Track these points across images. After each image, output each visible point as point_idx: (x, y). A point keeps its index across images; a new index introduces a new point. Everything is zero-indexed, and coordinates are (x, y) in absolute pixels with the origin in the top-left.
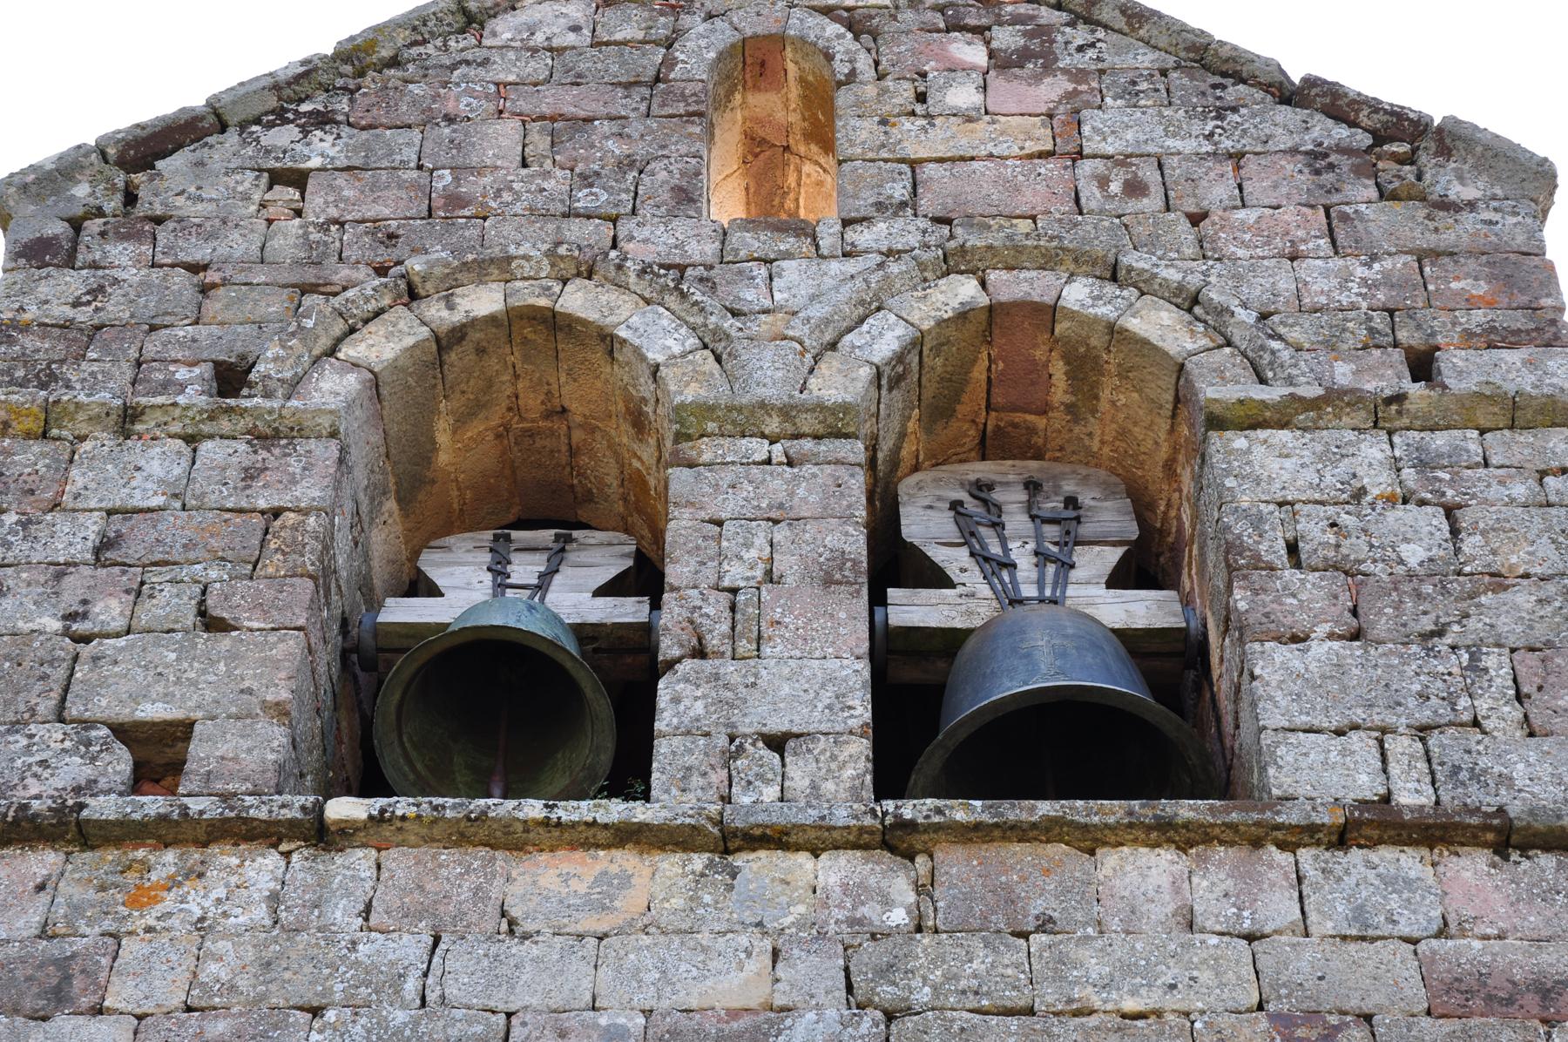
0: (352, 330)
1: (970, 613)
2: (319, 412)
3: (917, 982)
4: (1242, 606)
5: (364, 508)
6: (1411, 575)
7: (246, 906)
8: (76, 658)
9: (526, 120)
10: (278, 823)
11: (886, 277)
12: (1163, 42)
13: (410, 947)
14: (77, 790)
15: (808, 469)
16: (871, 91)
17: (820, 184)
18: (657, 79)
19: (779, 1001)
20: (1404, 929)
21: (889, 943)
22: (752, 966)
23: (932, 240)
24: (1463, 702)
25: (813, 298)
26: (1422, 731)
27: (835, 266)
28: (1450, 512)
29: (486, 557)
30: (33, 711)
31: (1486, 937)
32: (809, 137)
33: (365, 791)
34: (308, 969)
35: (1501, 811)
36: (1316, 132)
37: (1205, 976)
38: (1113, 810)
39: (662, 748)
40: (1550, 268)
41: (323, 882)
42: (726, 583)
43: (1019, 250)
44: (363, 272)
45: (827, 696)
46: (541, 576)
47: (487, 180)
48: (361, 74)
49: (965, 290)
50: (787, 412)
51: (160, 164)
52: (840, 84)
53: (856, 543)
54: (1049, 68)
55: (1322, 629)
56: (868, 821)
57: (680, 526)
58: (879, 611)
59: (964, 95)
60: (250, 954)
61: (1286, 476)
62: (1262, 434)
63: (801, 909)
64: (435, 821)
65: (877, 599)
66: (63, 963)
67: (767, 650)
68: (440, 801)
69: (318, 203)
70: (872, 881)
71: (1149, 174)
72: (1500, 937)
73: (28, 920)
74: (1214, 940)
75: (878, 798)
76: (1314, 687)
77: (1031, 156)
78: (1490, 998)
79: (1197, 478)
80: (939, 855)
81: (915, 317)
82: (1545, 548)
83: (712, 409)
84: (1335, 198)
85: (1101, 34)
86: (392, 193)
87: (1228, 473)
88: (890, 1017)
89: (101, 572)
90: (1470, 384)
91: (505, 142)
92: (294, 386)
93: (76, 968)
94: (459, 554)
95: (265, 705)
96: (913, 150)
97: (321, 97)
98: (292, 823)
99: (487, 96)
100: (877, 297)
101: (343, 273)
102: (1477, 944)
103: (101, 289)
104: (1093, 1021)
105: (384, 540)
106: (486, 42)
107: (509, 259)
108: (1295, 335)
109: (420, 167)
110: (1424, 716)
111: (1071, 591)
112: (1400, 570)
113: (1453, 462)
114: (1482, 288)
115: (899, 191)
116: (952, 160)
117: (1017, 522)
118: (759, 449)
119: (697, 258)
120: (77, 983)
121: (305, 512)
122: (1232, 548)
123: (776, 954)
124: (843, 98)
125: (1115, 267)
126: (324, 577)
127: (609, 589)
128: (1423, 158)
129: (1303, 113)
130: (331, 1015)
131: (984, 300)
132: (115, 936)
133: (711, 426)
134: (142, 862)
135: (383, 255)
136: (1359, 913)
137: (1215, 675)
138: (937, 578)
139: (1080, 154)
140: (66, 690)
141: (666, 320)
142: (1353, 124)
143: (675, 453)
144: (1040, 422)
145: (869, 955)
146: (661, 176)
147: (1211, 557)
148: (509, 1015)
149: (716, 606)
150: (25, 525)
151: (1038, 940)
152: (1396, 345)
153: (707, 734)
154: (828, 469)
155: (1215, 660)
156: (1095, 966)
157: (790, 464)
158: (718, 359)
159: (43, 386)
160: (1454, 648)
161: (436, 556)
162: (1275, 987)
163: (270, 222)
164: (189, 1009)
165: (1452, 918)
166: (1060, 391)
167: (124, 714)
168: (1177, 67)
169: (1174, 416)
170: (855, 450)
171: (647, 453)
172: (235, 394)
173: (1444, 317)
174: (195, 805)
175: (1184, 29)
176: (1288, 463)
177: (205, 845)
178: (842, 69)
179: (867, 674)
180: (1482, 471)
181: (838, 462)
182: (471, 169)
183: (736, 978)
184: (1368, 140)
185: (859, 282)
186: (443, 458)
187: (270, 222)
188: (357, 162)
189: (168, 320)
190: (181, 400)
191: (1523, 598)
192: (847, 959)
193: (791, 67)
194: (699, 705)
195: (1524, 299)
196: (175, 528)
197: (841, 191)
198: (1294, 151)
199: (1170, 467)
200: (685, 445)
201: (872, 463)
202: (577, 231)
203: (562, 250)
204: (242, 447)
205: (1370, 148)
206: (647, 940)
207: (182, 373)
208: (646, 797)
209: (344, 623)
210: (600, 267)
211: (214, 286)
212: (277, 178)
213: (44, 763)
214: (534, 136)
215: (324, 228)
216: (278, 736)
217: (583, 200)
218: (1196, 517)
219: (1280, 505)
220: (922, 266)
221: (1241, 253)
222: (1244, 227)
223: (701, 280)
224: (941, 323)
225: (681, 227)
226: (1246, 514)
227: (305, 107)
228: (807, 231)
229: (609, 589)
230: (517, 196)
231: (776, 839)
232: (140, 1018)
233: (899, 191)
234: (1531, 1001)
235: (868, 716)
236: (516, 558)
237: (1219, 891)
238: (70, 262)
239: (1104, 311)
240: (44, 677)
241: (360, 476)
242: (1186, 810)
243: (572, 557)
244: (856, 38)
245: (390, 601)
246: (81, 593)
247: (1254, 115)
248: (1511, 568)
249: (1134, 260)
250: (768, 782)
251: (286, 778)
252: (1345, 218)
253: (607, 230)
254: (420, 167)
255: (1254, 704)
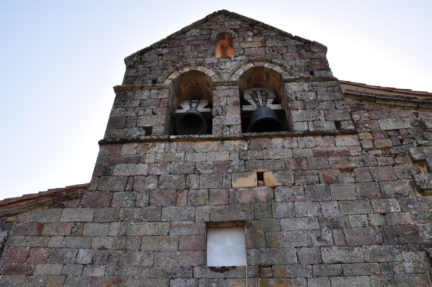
0: (170, 74)
1: (254, 108)
2: (166, 85)
3: (248, 157)
4: (290, 106)
5: (173, 98)
6: (311, 101)
7: (161, 150)
8: (137, 119)
9: (191, 45)
10: (164, 139)
11: (241, 64)
12: (276, 31)
13: (182, 154)
14: (139, 136)
15: (231, 90)
16: (237, 39)
17: (231, 52)
18: (209, 39)
19: (230, 160)
20: (311, 146)
21: (245, 152)
22: (227, 155)
23: (247, 59)
24: (318, 117)
25: (231, 67)
26: (313, 121)
27: (234, 63)
28: (316, 92)
29: (189, 104)
30: (133, 126)
31: (321, 147)
32: (229, 46)
33: (175, 135)
34: (169, 157)
35: (323, 131)
36: (297, 43)
37: (286, 154)
38: (273, 133)
39: (214, 128)
40: (327, 60)
41: (170, 146)
42: (221, 105)
43: (258, 59)
44: (171, 67)
45: (235, 120)
46: (196, 106)
47: (187, 53)
48: (170, 41)
49: (252, 65)
50: (228, 82)
51: (144, 54)
52: (233, 38)
53: (238, 99)
54: (261, 35)
55: (300, 108)
56: (241, 136)
57: (215, 98)
58: (241, 109)
59: (250, 39)
60: (162, 156)
61: (295, 88)
62: (291, 83)
63: (233, 148)
64: (184, 138)
65: (241, 107)
66: (139, 157)
67: (227, 114)
68: (184, 136)
69: (165, 58)
70: (242, 144)
71: (275, 49)
72: (323, 147)
73: (135, 152)
74: (287, 149)
75: (242, 133)
76: (299, 116)
77: (259, 47)
78: (321, 154)
79: (283, 89)
80: (251, 140)
81: (245, 69)
82: (328, 97)
83: (219, 82)
84: (300, 52)
85: (268, 31)
86: (174, 56)
87: (287, 88)
88: (245, 161)
89: (140, 108)
90: (318, 76)
91: (189, 48)
92: (163, 82)
93: (141, 158)
94: (185, 104)
95: (161, 124)
96: (244, 47)
97: (165, 44)
98: (166, 139)
99: (186, 43)
100: (239, 66)
101: (168, 67)
102: (320, 148)
103: (138, 71)
104: (271, 160)
105: (175, 102)
106: (186, 35)
107: (190, 64)
108: (295, 70)
109: (178, 52)
110: (313, 119)
111: (267, 105)
112: (310, 100)
113: (316, 86)
114: (319, 63)
115: (242, 52)
116: (249, 48)
117: (259, 96)
118: (224, 87)
119: (215, 62)
120: (141, 159)
121: (165, 99)
122: (288, 98)
123: (230, 154)
124: (234, 40)
125: (271, 61)
126: (168, 107)
127: (205, 107)
128: (311, 46)
129: (295, 41)
130: (173, 163)
131: (254, 66)
132: (145, 154)
133: (218, 85)
134: (148, 144)
135: (173, 64)
136: (305, 145)
137: (286, 115)
138: (249, 104)
139: (266, 47)
140: (137, 123)
141: (211, 71)
142: (301, 42)
143: (213, 89)
144: (262, 82)
145: (242, 153)
146: (210, 52)
147: (285, 100)
148: (195, 163)
149: (220, 109)
150: (130, 102)
151: (264, 150)
152: (308, 71)
153: (219, 126)
154: (234, 90)
155: (286, 113)
156: (272, 154)
157: (229, 89)
158: (219, 76)
159: (131, 84)
160: (317, 110)
161: (182, 104)
162: (295, 155)
163: (159, 61)
164: (155, 163)
165: (317, 145)
166: (265, 78)
167: (144, 126)
168: (278, 35)
169: (280, 81)
170: (237, 87)
171: (210, 89)
172: (155, 84)
173: (314, 67)
174: (154, 137)
175: (279, 30)
176: (295, 87)
177: (155, 142)
178: (233, 36)
179: (240, 117)
180: (320, 87)
181: (235, 89)
182: (184, 52)
183: (225, 157)
184: (303, 44)
185: (237, 65)
186: (182, 91)
187: (159, 61)
188: (170, 52)
189: (146, 74)
190: (148, 85)
191: (325, 103)
192: (239, 154)
193: (227, 36)
194: (218, 122)
195: (324, 64)
196: (149, 102)
197: (234, 53)
198: (294, 45)
199: (279, 88)
200: (215, 87)
201: (240, 89)
202: (199, 60)
203: (197, 62)
204: (156, 90)
205: (304, 45)
206: (213, 153)
207: (148, 81)
208: (212, 134)
209: (171, 113)
210: (202, 64)
211: (152, 70)
212: (160, 55)
213: (135, 132)
214: (193, 47)
215: (166, 61)
216: (163, 128)
217: (199, 55)
218: (283, 94)
219: (294, 92)
220: (245, 62)
221: (288, 59)
222: (288, 56)
223: (216, 65)
224: (248, 70)
225: (213, 58)
226: (290, 94)
227: (163, 46)
228: (230, 58)
229: (205, 107)
230: (191, 55)
231: (229, 139)
232: (149, 164)
233: (242, 52)
234: (326, 154)
235: (241, 122)
236: (193, 104)
237: (287, 143)
238: (134, 68)
239: (270, 67)
240: (134, 121)
241: (172, 93)
242: (283, 133)
243: (200, 103)
244: (235, 32)
245: (177, 110)
246: (138, 110)
247: (288, 41)
248: (324, 99)
249: (274, 60)
250: (228, 131)
251: (165, 133)
252: (301, 54)
253: (203, 59)
254: (178, 52)
255: (291, 119)
